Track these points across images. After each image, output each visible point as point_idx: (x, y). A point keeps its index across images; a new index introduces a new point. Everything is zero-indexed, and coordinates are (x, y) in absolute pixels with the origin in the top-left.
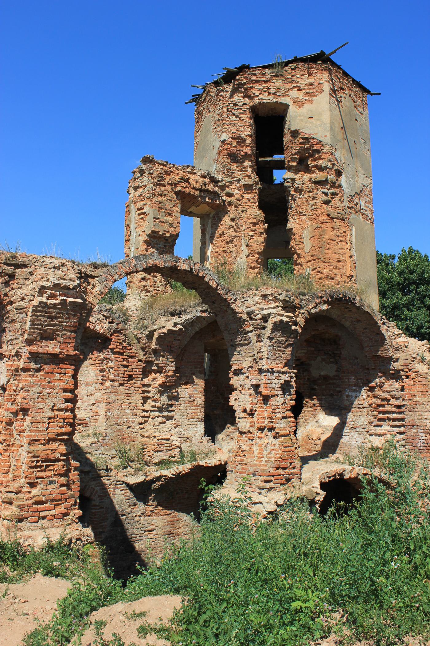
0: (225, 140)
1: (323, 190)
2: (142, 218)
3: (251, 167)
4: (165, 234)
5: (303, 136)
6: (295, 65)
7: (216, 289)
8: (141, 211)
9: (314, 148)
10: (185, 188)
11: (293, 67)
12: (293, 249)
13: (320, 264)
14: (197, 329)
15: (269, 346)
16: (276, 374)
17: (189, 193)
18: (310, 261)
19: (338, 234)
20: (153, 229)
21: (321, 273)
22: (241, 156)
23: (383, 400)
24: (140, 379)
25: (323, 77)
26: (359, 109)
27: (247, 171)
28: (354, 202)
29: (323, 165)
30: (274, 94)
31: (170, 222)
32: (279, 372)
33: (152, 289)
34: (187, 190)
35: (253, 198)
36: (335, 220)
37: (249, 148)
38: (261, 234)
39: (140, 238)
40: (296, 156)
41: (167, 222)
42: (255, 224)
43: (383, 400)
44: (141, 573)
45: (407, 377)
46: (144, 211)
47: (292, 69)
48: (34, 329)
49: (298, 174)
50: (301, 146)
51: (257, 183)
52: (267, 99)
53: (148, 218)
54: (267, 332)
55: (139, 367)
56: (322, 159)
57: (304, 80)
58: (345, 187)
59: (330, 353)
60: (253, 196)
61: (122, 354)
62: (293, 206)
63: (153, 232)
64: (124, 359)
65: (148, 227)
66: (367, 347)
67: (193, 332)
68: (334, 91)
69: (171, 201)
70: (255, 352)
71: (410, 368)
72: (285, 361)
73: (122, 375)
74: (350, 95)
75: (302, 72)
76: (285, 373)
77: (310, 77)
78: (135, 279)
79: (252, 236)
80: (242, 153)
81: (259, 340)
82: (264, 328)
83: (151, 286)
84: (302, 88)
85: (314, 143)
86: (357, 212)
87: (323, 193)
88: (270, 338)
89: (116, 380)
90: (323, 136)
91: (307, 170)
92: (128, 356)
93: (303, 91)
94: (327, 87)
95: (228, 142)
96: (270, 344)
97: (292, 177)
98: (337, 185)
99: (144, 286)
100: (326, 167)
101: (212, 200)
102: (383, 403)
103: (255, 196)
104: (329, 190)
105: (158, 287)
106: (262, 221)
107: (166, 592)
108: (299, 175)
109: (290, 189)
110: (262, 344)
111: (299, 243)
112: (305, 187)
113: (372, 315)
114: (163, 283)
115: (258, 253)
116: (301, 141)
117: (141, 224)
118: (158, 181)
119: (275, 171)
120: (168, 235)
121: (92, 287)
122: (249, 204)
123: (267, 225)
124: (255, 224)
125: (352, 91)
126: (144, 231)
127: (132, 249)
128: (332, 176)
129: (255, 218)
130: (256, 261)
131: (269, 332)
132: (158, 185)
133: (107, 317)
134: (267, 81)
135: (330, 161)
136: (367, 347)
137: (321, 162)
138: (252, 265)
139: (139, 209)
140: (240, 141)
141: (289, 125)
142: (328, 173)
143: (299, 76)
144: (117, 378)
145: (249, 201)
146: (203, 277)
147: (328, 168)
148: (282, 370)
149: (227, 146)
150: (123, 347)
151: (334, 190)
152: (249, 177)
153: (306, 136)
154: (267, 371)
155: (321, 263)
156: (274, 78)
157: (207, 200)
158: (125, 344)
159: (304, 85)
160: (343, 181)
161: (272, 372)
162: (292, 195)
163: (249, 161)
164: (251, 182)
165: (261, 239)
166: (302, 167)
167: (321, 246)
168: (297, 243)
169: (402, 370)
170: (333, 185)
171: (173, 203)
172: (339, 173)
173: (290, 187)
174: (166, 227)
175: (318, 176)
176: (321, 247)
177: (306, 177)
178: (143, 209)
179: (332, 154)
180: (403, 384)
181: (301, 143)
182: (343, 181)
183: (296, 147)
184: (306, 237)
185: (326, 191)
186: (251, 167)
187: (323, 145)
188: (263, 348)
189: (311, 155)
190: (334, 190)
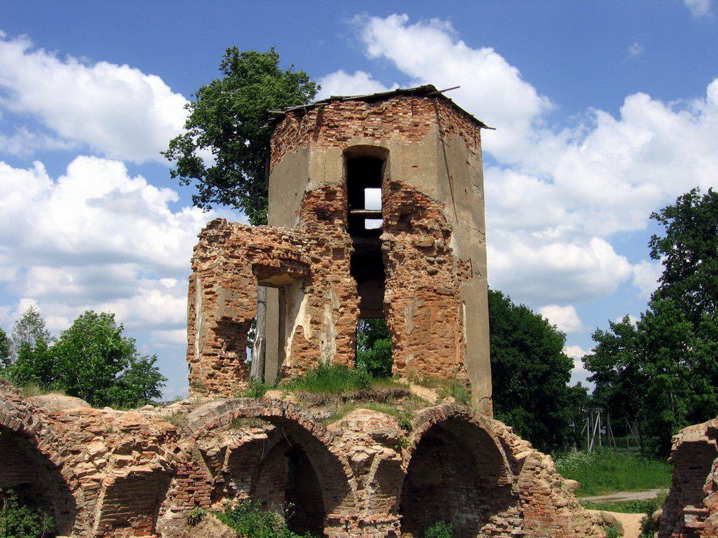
0: (311, 192)
1: (428, 258)
2: (210, 299)
3: (341, 225)
4: (239, 320)
5: (405, 190)
6: (397, 101)
7: (312, 431)
8: (209, 290)
9: (418, 205)
10: (262, 259)
11: (395, 103)
12: (391, 329)
13: (424, 350)
14: (278, 441)
15: (372, 494)
16: (379, 526)
18: (411, 345)
19: (446, 313)
20: (225, 315)
21: (425, 362)
22: (331, 212)
23: (499, 526)
24: (208, 506)
25: (429, 118)
26: (471, 148)
27: (337, 230)
28: (464, 266)
29: (429, 226)
30: (373, 135)
31: (245, 304)
32: (383, 523)
33: (221, 388)
34: (266, 262)
35: (344, 265)
37: (340, 203)
38: (353, 311)
39: (208, 323)
40: (397, 214)
41: (242, 304)
42: (345, 298)
43: (499, 526)
45: (527, 502)
46: (213, 289)
47: (394, 106)
48: (105, 518)
49: (398, 234)
50: (402, 201)
51: (348, 245)
52: (365, 141)
53: (218, 300)
54: (370, 478)
55: (207, 491)
56: (428, 218)
57: (407, 119)
58: (455, 253)
59: (435, 455)
60: (344, 263)
61: (187, 476)
62: (392, 274)
63: (224, 318)
64: (189, 483)
65: (219, 311)
66: (480, 463)
67: (273, 445)
68: (442, 133)
69: (245, 277)
70: (356, 501)
71: (531, 491)
72: (390, 508)
73: (186, 504)
74: (461, 134)
75: (405, 110)
76: (389, 522)
77: (414, 116)
78: (201, 375)
79: (342, 313)
80: (331, 209)
81: (360, 487)
82: (367, 472)
83: (221, 385)
84: (405, 129)
85: (418, 199)
86: (467, 278)
87: (428, 261)
88: (373, 485)
89: (179, 511)
90: (430, 190)
91: (410, 229)
92: (194, 479)
93: (407, 133)
94: (434, 129)
95: (315, 195)
96: (373, 492)
97: (392, 240)
98: (445, 250)
99: (212, 385)
100: (432, 229)
101: (295, 269)
102: (499, 530)
104: (435, 257)
105: (229, 386)
106: (355, 294)
108: (400, 236)
109: (389, 254)
110: (363, 491)
111: (399, 322)
112: (406, 253)
113: (488, 431)
114: (235, 378)
116: (403, 195)
117: (209, 306)
118: (231, 253)
119: (366, 220)
120: (242, 320)
123: (360, 298)
124: (345, 298)
125: (463, 127)
126: (213, 316)
127: (198, 336)
128: (439, 240)
129: (346, 291)
130: (348, 344)
131: (373, 478)
132: (231, 257)
134: (363, 119)
135: (437, 221)
136: (480, 463)
137: (426, 222)
138: (343, 349)
139: (206, 287)
140: (330, 194)
141: (389, 175)
142: (435, 236)
143: (401, 114)
144: (182, 508)
145: (339, 268)
146: (297, 421)
147: (435, 230)
148: (386, 520)
149: (312, 199)
150: (187, 468)
151: (441, 258)
152: (339, 237)
153: (409, 190)
154: (370, 524)
155: (425, 350)
156: (371, 116)
157: (289, 270)
158: (190, 463)
159: (407, 126)
160: (452, 243)
161: (375, 524)
162: (392, 261)
163: (340, 219)
164: (341, 244)
166: (403, 226)
167: (424, 326)
168: (396, 322)
169: (522, 493)
170: (441, 251)
171: (248, 280)
172: (447, 234)
173: (388, 251)
174: (240, 311)
175: (423, 238)
176: (426, 331)
177: (408, 238)
178: (212, 286)
179: (439, 212)
180: (523, 510)
181: (403, 198)
182: (452, 243)
183: (397, 203)
184: (408, 315)
185: (432, 259)
186: (341, 225)
187: (429, 202)
188: (365, 496)
189: (415, 212)
190: (441, 258)
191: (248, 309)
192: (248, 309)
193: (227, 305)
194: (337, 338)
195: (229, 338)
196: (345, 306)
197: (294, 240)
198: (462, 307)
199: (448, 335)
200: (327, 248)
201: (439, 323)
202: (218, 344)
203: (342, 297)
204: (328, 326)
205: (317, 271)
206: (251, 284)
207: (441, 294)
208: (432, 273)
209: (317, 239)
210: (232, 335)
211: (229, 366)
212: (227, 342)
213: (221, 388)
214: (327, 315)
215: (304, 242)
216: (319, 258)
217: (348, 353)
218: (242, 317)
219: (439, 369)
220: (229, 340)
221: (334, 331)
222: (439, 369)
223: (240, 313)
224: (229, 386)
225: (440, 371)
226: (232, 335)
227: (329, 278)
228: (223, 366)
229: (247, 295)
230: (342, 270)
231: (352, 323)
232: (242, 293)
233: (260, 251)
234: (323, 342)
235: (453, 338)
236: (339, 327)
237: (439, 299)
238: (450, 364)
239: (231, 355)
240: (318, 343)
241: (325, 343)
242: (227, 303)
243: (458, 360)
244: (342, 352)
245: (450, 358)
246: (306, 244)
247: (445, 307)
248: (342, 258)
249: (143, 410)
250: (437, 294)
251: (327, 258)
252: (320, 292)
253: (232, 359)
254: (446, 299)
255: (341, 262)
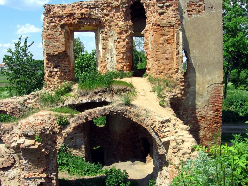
4: (54, 53)
10: (67, 21)
17: (71, 23)
31: (57, 45)
33: (51, 86)
35: (120, 15)
36: (164, 28)
38: (124, 40)
41: (55, 46)
42: (120, 33)
44: (42, 129)
69: (56, 32)
83: (51, 84)
103: (121, 13)
107: (27, 49)
114: (59, 81)
115: (123, 53)
121: (161, 126)
122: (118, 19)
129: (120, 30)
130: (122, 58)
132: (50, 23)
133: (33, 109)
138: (120, 61)
145: (118, 17)
165: (124, 43)
171: (59, 33)
191: (59, 48)
192: (59, 48)
193: (47, 47)
194: (117, 56)
195: (54, 62)
196: (120, 38)
197: (92, 6)
198: (178, 33)
199: (168, 52)
200: (112, 7)
201: (162, 45)
202: (49, 65)
203: (118, 33)
204: (111, 50)
205: (106, 21)
206: (61, 35)
207: (163, 27)
208: (161, 14)
209: (107, 3)
210: (56, 61)
211: (56, 75)
212: (53, 64)
213: (51, 86)
214: (111, 44)
215: (99, 6)
216: (108, 13)
217: (123, 63)
218: (56, 52)
219: (162, 72)
220: (55, 63)
221: (115, 52)
222: (162, 72)
223: (55, 50)
224: (55, 84)
225: (162, 74)
226: (56, 61)
227: (113, 23)
228: (53, 75)
229: (58, 41)
230: (120, 18)
231: (123, 47)
232: (55, 40)
233: (65, 17)
234: (108, 59)
235: (172, 53)
236: (118, 50)
237: (161, 30)
238: (169, 69)
239: (56, 70)
240: (105, 59)
241: (110, 59)
242: (47, 46)
243: (175, 66)
244: (119, 63)
245: (169, 65)
246: (101, 7)
247: (166, 35)
248: (119, 11)
249: (11, 98)
250: (161, 27)
251: (112, 12)
252: (106, 32)
253: (57, 72)
254: (166, 30)
255: (119, 14)
